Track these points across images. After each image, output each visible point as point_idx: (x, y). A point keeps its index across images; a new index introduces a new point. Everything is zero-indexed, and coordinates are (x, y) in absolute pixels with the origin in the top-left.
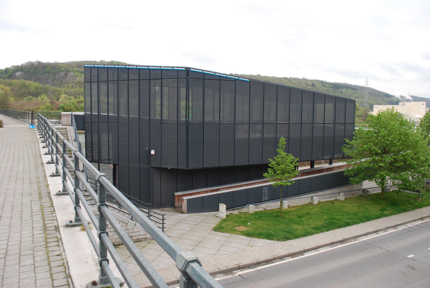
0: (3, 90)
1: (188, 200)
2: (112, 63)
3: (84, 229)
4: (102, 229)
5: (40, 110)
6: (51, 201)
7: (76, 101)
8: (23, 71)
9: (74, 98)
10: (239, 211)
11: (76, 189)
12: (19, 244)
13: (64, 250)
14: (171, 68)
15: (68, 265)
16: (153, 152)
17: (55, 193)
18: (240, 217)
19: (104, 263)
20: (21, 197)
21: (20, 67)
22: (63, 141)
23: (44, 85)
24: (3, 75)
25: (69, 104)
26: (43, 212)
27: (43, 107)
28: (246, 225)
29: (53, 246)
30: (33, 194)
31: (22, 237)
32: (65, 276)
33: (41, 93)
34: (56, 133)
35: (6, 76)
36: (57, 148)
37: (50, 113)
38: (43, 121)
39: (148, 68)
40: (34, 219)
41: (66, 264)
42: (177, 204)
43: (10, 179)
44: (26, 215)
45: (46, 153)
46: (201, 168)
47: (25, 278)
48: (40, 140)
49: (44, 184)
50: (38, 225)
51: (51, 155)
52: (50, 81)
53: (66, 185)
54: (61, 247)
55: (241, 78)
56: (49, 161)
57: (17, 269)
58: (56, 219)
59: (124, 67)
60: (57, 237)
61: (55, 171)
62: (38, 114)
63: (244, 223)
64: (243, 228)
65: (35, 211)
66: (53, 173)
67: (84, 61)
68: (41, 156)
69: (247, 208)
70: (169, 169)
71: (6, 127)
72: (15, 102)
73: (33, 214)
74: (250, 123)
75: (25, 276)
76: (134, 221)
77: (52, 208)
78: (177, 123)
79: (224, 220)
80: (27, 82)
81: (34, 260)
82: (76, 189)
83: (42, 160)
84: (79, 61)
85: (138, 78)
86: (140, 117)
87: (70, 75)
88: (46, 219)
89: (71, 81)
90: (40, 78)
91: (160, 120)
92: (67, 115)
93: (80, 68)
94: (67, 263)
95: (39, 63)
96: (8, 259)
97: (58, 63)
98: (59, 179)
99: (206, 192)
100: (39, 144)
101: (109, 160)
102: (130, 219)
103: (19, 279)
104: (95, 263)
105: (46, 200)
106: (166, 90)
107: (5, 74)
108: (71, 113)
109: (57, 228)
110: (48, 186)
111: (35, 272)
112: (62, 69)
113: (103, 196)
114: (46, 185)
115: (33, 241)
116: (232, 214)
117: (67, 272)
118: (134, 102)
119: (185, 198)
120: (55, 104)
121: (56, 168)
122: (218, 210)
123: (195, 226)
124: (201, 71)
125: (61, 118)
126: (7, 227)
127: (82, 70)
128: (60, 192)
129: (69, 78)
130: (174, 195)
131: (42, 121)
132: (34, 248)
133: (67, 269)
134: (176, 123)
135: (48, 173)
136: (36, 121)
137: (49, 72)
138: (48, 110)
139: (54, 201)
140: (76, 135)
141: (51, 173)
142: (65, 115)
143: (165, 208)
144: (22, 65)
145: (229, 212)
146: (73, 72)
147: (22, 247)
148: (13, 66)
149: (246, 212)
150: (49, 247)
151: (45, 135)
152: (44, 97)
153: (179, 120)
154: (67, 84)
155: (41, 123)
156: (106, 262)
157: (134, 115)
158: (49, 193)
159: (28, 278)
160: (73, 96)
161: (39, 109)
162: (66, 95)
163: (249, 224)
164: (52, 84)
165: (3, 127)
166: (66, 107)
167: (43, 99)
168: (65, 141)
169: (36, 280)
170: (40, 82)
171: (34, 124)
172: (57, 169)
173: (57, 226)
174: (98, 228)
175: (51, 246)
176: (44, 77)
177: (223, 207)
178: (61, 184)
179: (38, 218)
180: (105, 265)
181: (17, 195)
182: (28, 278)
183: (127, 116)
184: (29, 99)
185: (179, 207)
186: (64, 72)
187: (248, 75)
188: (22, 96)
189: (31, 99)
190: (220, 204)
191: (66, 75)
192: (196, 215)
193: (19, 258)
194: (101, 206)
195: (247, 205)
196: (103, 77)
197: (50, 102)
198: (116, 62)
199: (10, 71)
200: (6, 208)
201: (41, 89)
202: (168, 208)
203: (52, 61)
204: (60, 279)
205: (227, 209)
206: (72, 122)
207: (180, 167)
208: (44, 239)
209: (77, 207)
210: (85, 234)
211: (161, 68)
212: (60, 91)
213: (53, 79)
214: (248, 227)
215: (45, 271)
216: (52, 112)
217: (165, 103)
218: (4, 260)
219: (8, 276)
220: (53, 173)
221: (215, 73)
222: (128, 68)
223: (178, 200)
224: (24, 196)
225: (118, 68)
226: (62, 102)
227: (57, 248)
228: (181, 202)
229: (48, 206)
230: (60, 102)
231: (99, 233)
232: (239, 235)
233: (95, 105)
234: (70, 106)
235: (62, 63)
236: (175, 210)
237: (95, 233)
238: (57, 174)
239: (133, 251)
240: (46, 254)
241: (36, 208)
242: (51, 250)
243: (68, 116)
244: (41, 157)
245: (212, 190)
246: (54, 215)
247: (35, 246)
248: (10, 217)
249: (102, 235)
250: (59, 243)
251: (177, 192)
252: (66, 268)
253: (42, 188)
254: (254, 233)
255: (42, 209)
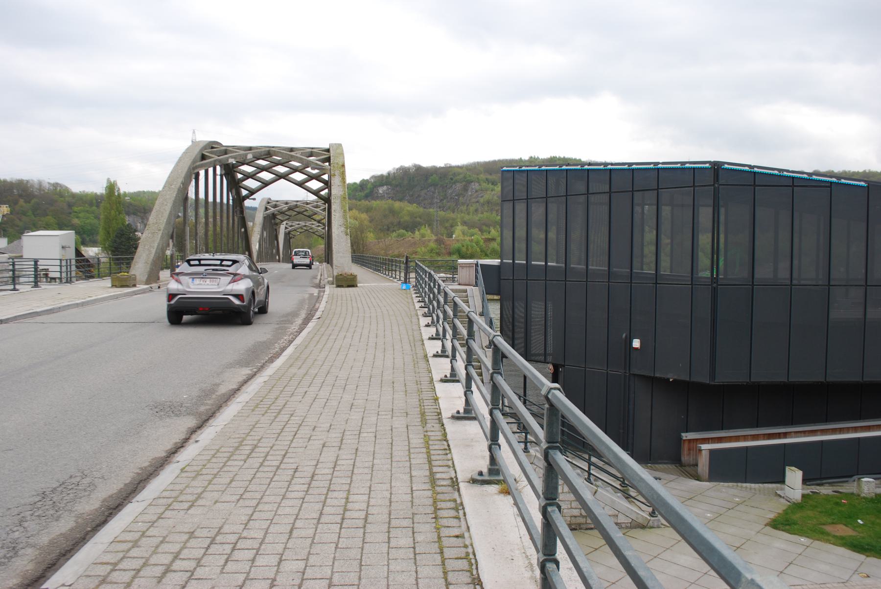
0: (356, 220)
1: (712, 452)
2: (552, 161)
3: (507, 492)
4: (549, 496)
5: (418, 255)
6: (442, 430)
7: (483, 237)
8: (391, 185)
9: (479, 232)
10: (835, 488)
11: (494, 410)
12: (389, 504)
13: (468, 528)
14: (679, 166)
15: (476, 559)
16: (636, 343)
17: (450, 415)
18: (837, 504)
19: (550, 568)
20: (390, 416)
21: (385, 178)
22: (467, 315)
23: (425, 210)
24: (357, 194)
25: (469, 243)
26: (428, 448)
27: (423, 249)
28: (851, 524)
29: (447, 516)
30: (411, 413)
31: (393, 493)
32: (469, 580)
33: (420, 224)
34: (453, 299)
35: (362, 194)
36: (454, 328)
37: (435, 262)
38: (426, 276)
39: (628, 168)
40: (413, 461)
41: (471, 556)
42: (685, 458)
43: (370, 381)
44: (400, 452)
45: (431, 336)
46: (745, 384)
47: (398, 572)
48: (421, 312)
49: (429, 395)
50: (421, 473)
51: (442, 341)
52: (436, 200)
53: (471, 401)
54: (463, 523)
55: (845, 179)
56: (437, 352)
57: (384, 552)
58: (452, 466)
59: (579, 167)
60: (455, 501)
61: (449, 371)
62: (416, 263)
63: (848, 518)
64: (843, 530)
65: (414, 446)
66: (446, 376)
67: (500, 161)
68: (423, 341)
69: (856, 483)
70: (671, 380)
71: (361, 286)
72: (376, 241)
73: (412, 451)
74: (868, 284)
75: (398, 568)
76: (592, 484)
77: (445, 443)
78: (692, 282)
79: (796, 507)
80: (397, 205)
81: (414, 540)
82: (494, 410)
83: (424, 350)
84: (489, 162)
85: (607, 189)
86: (611, 270)
87: (472, 189)
88: (434, 463)
89: (474, 200)
90: (419, 196)
91: (655, 276)
92: (468, 265)
93: (491, 174)
94: (474, 555)
95: (418, 168)
96: (369, 531)
97: (451, 167)
98: (458, 389)
99: (755, 437)
100: (418, 319)
101: (545, 355)
102: (585, 479)
103: (388, 572)
104: (527, 562)
105: (433, 427)
106: (666, 211)
107: (361, 191)
108: (476, 260)
109: (454, 483)
110: (436, 399)
111: (415, 563)
112: (458, 177)
113: (554, 430)
114: (433, 398)
115: (412, 502)
116: (817, 493)
117: (475, 572)
118: (599, 239)
119: (705, 447)
120: (444, 244)
121: (452, 367)
122: (782, 481)
123: (725, 510)
124: (747, 168)
125: (457, 271)
126: (366, 471)
127: (497, 177)
128: (458, 412)
129: (470, 193)
130: (680, 438)
131: (424, 276)
132: (413, 517)
133: (474, 567)
134: (690, 283)
135: (437, 376)
136: (413, 275)
137: (435, 185)
138: (431, 256)
139: (447, 430)
140: (484, 303)
141: (443, 376)
142: (464, 266)
143: (660, 463)
144: (389, 174)
145: (808, 489)
146: (479, 182)
147: (392, 511)
148: (373, 177)
149: (852, 494)
150: (441, 518)
151: (431, 302)
152: (426, 231)
153: (695, 276)
154: (467, 206)
155: (423, 279)
156: (555, 566)
157: (598, 266)
158: (440, 414)
159: (403, 571)
160: (477, 229)
161: (416, 253)
162: (465, 228)
163: (859, 521)
164: (440, 207)
165: (357, 286)
166: (464, 249)
167: (423, 236)
168: (471, 315)
169: (417, 579)
170: (419, 204)
171: (409, 281)
172: (453, 369)
173: (454, 479)
174: (541, 493)
175: (444, 516)
176: (426, 194)
177: (794, 476)
178: (460, 397)
179: (420, 459)
180: (552, 571)
181: (383, 413)
182: (403, 571)
183: (584, 267)
184: (399, 236)
185: (689, 465)
186: (461, 183)
187: (858, 173)
188: (388, 229)
189: (402, 236)
190: (787, 468)
191: (465, 189)
192: (728, 487)
193: (389, 532)
194: (550, 451)
195: (856, 477)
196: (538, 190)
197: (436, 241)
198: (560, 159)
199: (369, 186)
200: (365, 435)
201: (420, 218)
202: (665, 466)
203: (440, 163)
204: (460, 584)
205: (805, 481)
206: (476, 278)
207: (697, 378)
208: (431, 501)
209: (493, 446)
210: (509, 500)
211: (656, 167)
212: (454, 219)
213: (442, 198)
214: (857, 529)
215: (434, 563)
216: (439, 259)
217: (665, 241)
218: (362, 530)
219: (368, 563)
220: (446, 376)
221: (779, 170)
222: (588, 170)
223: (689, 450)
224: (394, 414)
225: (567, 170)
226: (458, 241)
227: (454, 522)
228: (696, 455)
229: (437, 438)
230: (453, 240)
231: (543, 505)
232: (834, 544)
233: (521, 246)
234: (472, 247)
235: (458, 167)
236: (681, 471)
237: (533, 505)
238: (452, 378)
239: (623, 552)
240: (435, 530)
241: (417, 440)
242: (444, 525)
243: (466, 267)
244: (423, 344)
245: (769, 434)
246: (449, 456)
247: (416, 512)
248: (372, 453)
249: (549, 509)
250: (458, 513)
251: (687, 432)
252: (472, 565)
253: (426, 403)
254: (872, 546)
255: (427, 442)
